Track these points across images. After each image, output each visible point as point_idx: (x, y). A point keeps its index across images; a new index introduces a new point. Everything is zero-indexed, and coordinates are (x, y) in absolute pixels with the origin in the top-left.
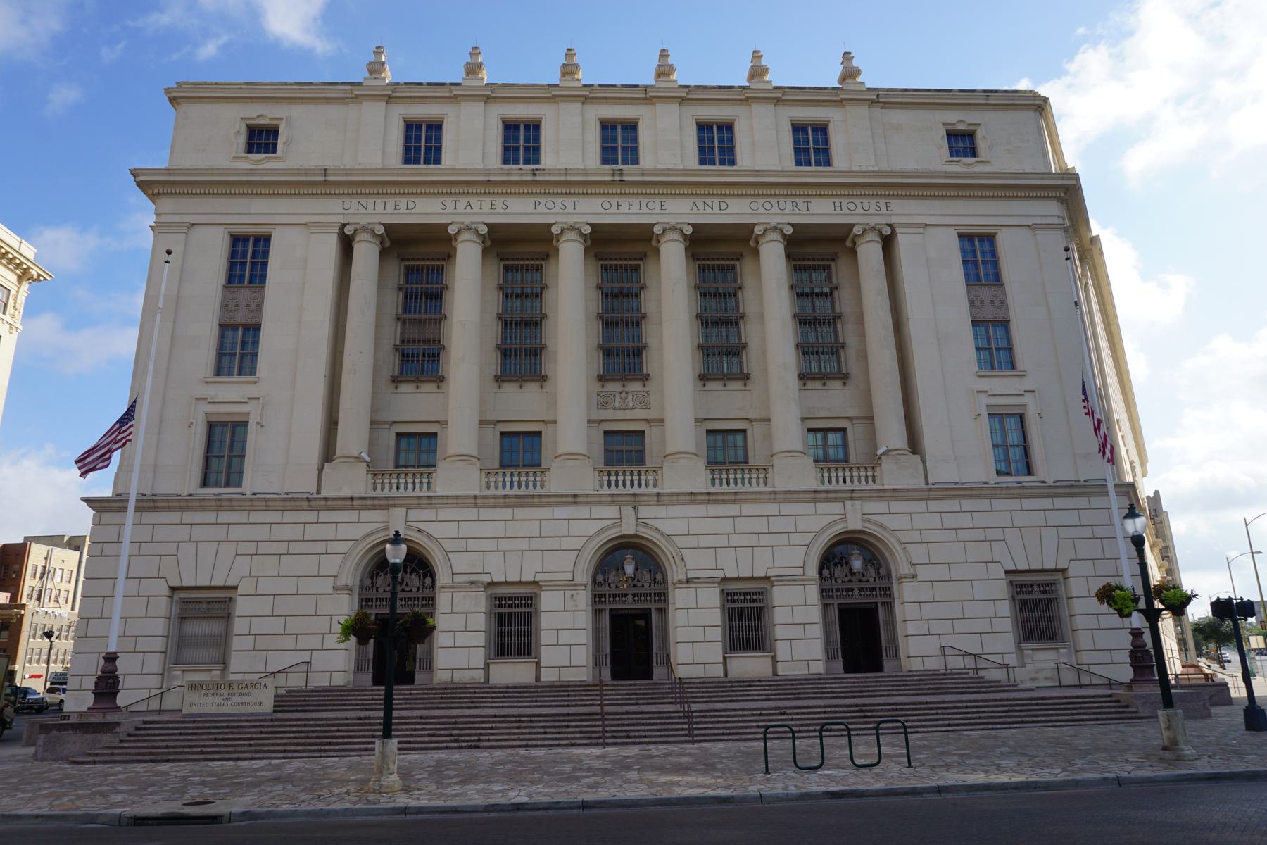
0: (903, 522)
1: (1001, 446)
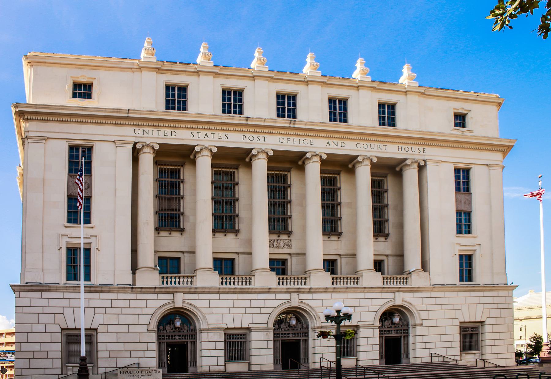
0: (419, 301)
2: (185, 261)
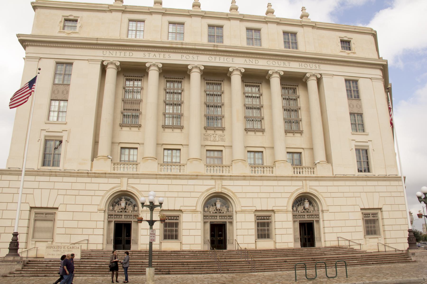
2: (226, 152)
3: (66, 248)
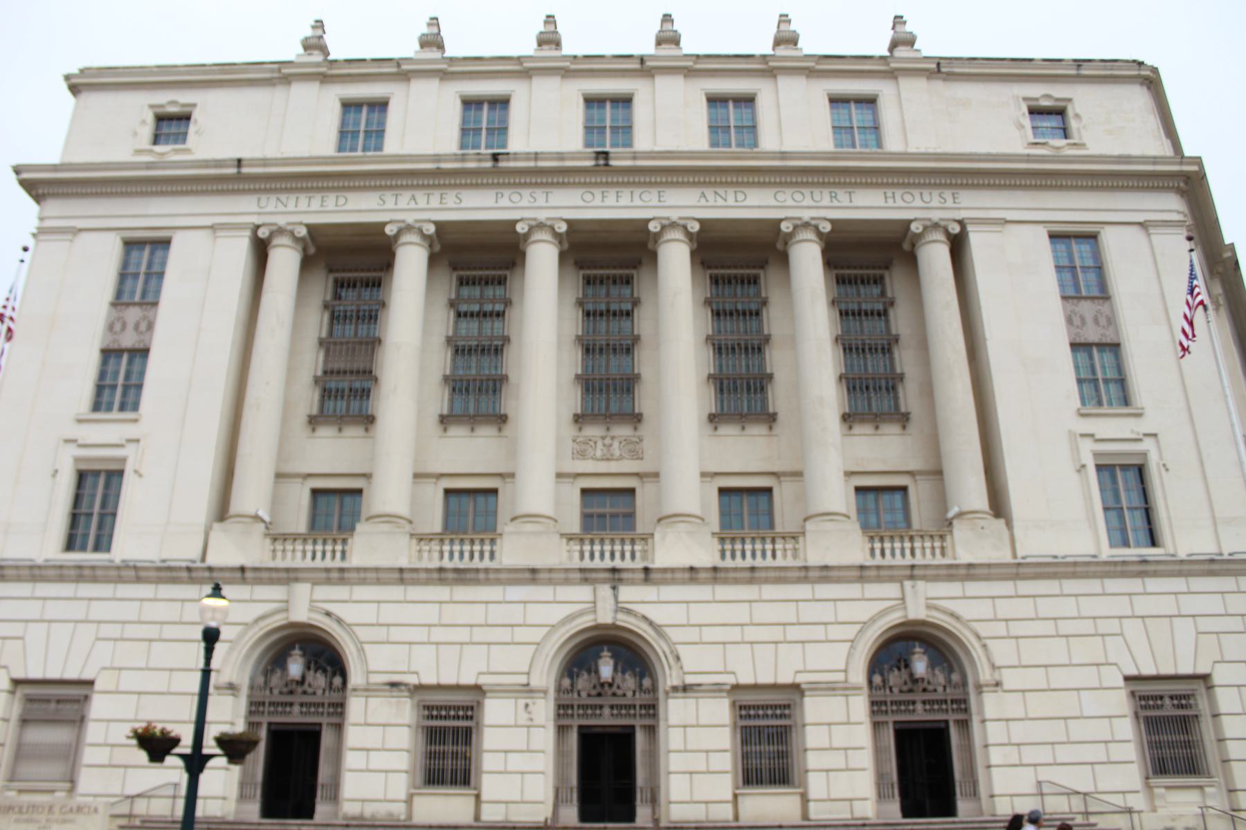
1: (1112, 508)
2: (783, 495)
3: (56, 809)
